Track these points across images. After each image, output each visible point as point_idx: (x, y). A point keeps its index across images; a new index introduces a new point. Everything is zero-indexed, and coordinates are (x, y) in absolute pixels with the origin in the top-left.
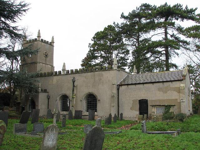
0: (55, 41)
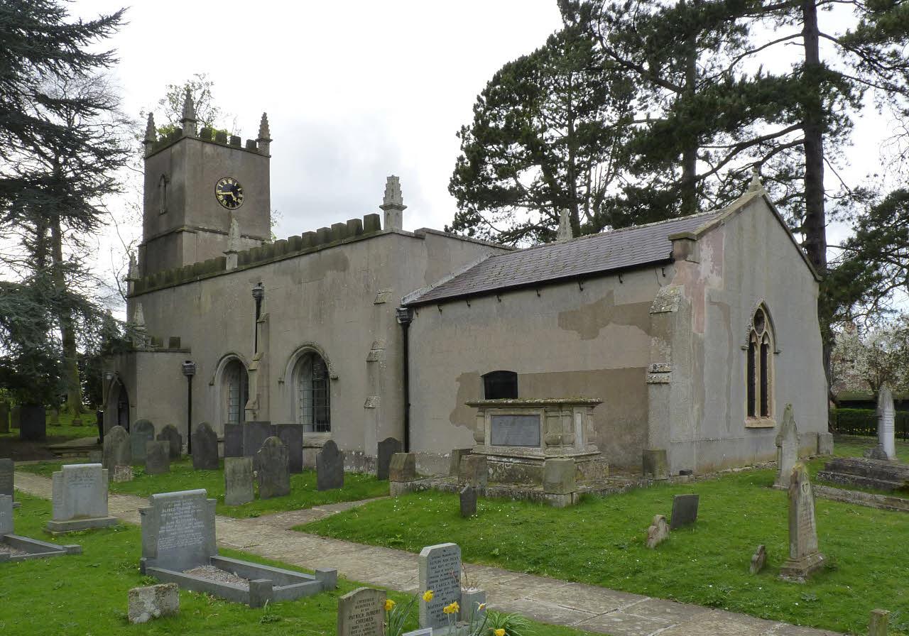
0: (273, 133)
